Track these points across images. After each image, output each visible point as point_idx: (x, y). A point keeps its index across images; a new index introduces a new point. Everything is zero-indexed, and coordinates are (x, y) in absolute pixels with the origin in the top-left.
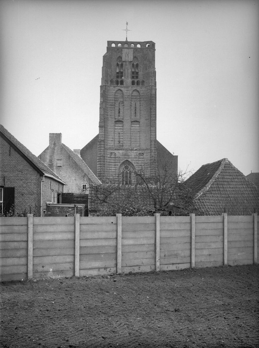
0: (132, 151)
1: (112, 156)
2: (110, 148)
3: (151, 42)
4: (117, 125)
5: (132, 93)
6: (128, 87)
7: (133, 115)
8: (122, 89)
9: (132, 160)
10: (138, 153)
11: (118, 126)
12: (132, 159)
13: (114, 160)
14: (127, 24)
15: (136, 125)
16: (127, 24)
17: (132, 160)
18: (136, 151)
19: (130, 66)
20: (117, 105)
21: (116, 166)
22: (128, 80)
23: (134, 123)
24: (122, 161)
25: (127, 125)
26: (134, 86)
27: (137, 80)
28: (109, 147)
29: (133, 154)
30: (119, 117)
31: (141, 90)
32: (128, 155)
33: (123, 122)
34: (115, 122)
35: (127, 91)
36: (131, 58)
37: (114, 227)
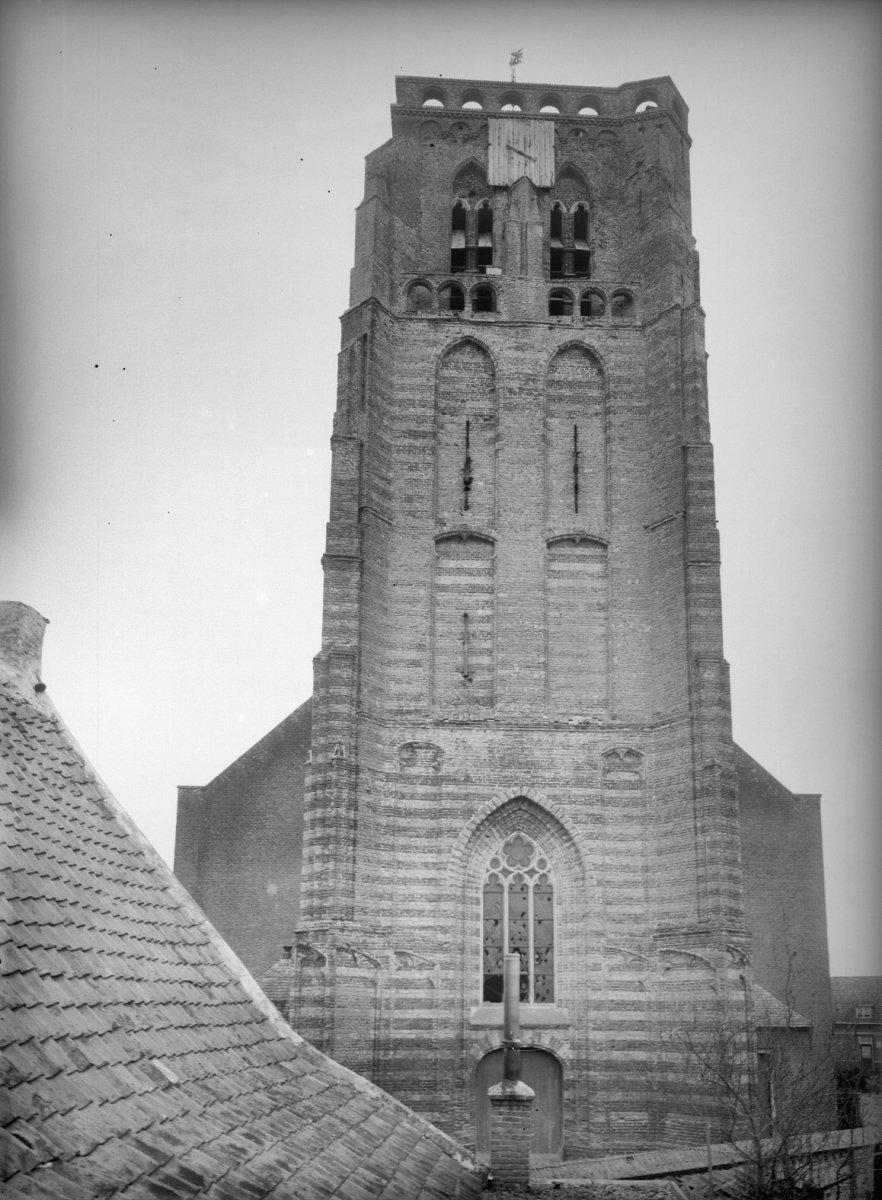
1: (414, 771)
8: (486, 336)
10: (601, 748)
11: (460, 571)
12: (558, 791)
20: (453, 433)
26: (566, 319)
28: (393, 705)
35: (517, 349)
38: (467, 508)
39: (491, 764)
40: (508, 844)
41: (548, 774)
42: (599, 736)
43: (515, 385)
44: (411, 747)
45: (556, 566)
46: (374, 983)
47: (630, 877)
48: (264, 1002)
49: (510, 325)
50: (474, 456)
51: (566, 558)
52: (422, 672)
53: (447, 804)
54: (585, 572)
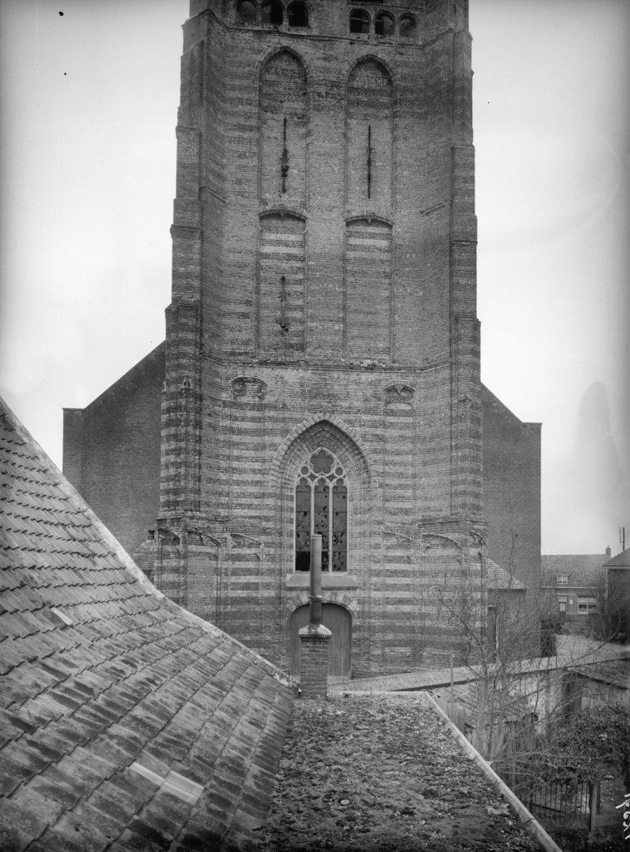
0: (354, 376)
1: (244, 400)
4: (273, 236)
5: (352, 76)
7: (358, 188)
8: (301, 48)
10: (384, 384)
11: (279, 243)
12: (352, 417)
13: (253, 419)
18: (372, 377)
21: (268, 453)
32: (332, 397)
35: (325, 59)
38: (284, 191)
39: (303, 394)
41: (345, 404)
44: (242, 381)
46: (216, 557)
51: (361, 235)
52: (249, 323)
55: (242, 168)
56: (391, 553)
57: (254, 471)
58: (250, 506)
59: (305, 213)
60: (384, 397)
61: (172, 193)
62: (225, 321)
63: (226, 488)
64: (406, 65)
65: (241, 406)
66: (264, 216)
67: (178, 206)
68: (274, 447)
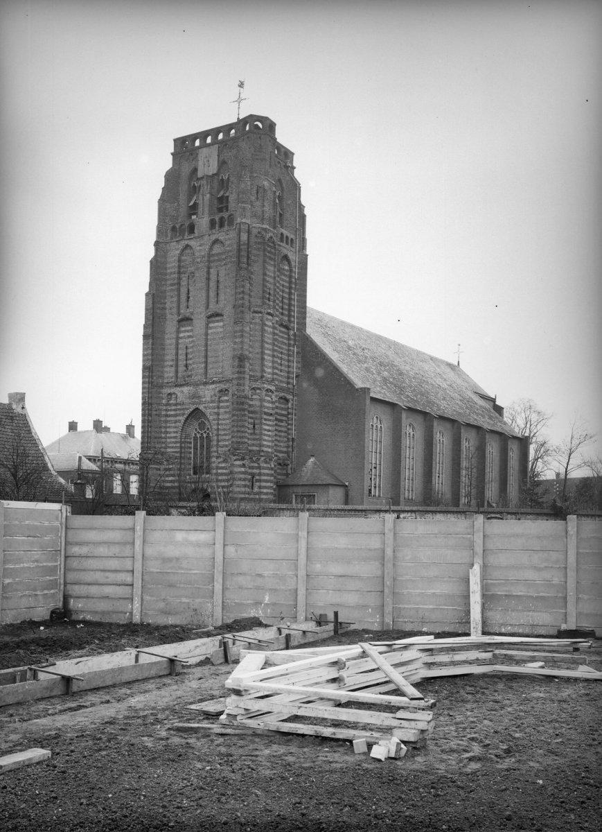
0: (207, 387)
1: (171, 402)
2: (168, 383)
3: (267, 118)
5: (211, 249)
6: (201, 237)
8: (192, 243)
9: (205, 407)
10: (218, 389)
11: (185, 331)
12: (206, 405)
14: (241, 85)
15: (216, 324)
16: (241, 85)
17: (205, 407)
18: (213, 386)
19: (209, 187)
21: (178, 424)
22: (202, 221)
23: (214, 319)
24: (187, 412)
25: (199, 323)
26: (214, 231)
27: (228, 213)
28: (166, 381)
29: (208, 392)
30: (188, 311)
31: (227, 237)
32: (199, 397)
33: (192, 320)
34: (179, 321)
35: (200, 246)
36: (213, 168)
37: (490, 546)
38: (188, 308)
39: (189, 398)
40: (199, 423)
41: (204, 400)
42: (218, 385)
43: (199, 260)
44: (170, 394)
45: (211, 325)
46: (160, 470)
47: (225, 432)
48: (388, 597)
49: (198, 237)
50: (190, 288)
51: (214, 322)
53: (178, 412)
54: (218, 326)
55: (172, 302)
56: (220, 465)
57: (174, 432)
58: (173, 447)
59: (192, 317)
60: (218, 395)
61: (143, 322)
62: (166, 369)
63: (164, 440)
64: (229, 239)
65: (170, 405)
66: (209, 317)
67: (145, 327)
68: (180, 421)
